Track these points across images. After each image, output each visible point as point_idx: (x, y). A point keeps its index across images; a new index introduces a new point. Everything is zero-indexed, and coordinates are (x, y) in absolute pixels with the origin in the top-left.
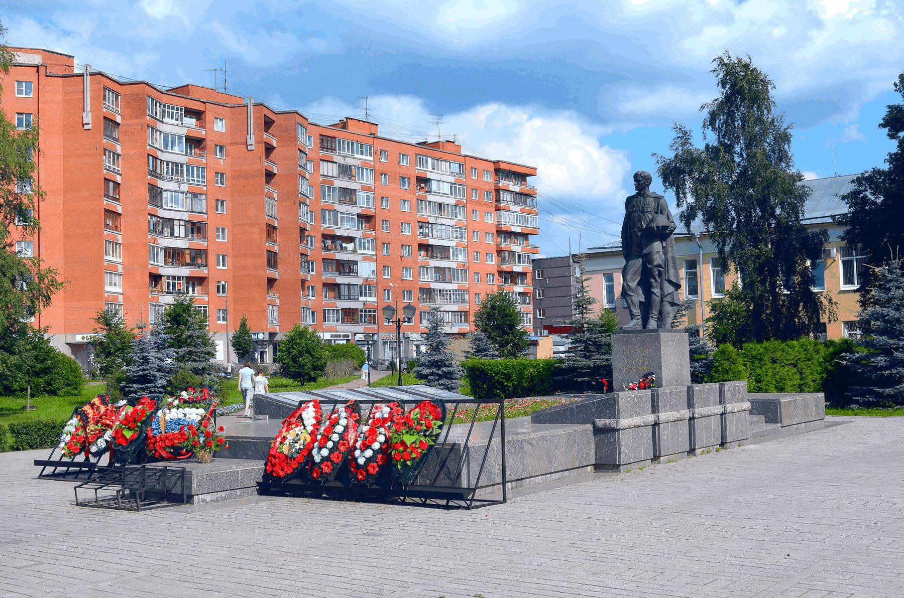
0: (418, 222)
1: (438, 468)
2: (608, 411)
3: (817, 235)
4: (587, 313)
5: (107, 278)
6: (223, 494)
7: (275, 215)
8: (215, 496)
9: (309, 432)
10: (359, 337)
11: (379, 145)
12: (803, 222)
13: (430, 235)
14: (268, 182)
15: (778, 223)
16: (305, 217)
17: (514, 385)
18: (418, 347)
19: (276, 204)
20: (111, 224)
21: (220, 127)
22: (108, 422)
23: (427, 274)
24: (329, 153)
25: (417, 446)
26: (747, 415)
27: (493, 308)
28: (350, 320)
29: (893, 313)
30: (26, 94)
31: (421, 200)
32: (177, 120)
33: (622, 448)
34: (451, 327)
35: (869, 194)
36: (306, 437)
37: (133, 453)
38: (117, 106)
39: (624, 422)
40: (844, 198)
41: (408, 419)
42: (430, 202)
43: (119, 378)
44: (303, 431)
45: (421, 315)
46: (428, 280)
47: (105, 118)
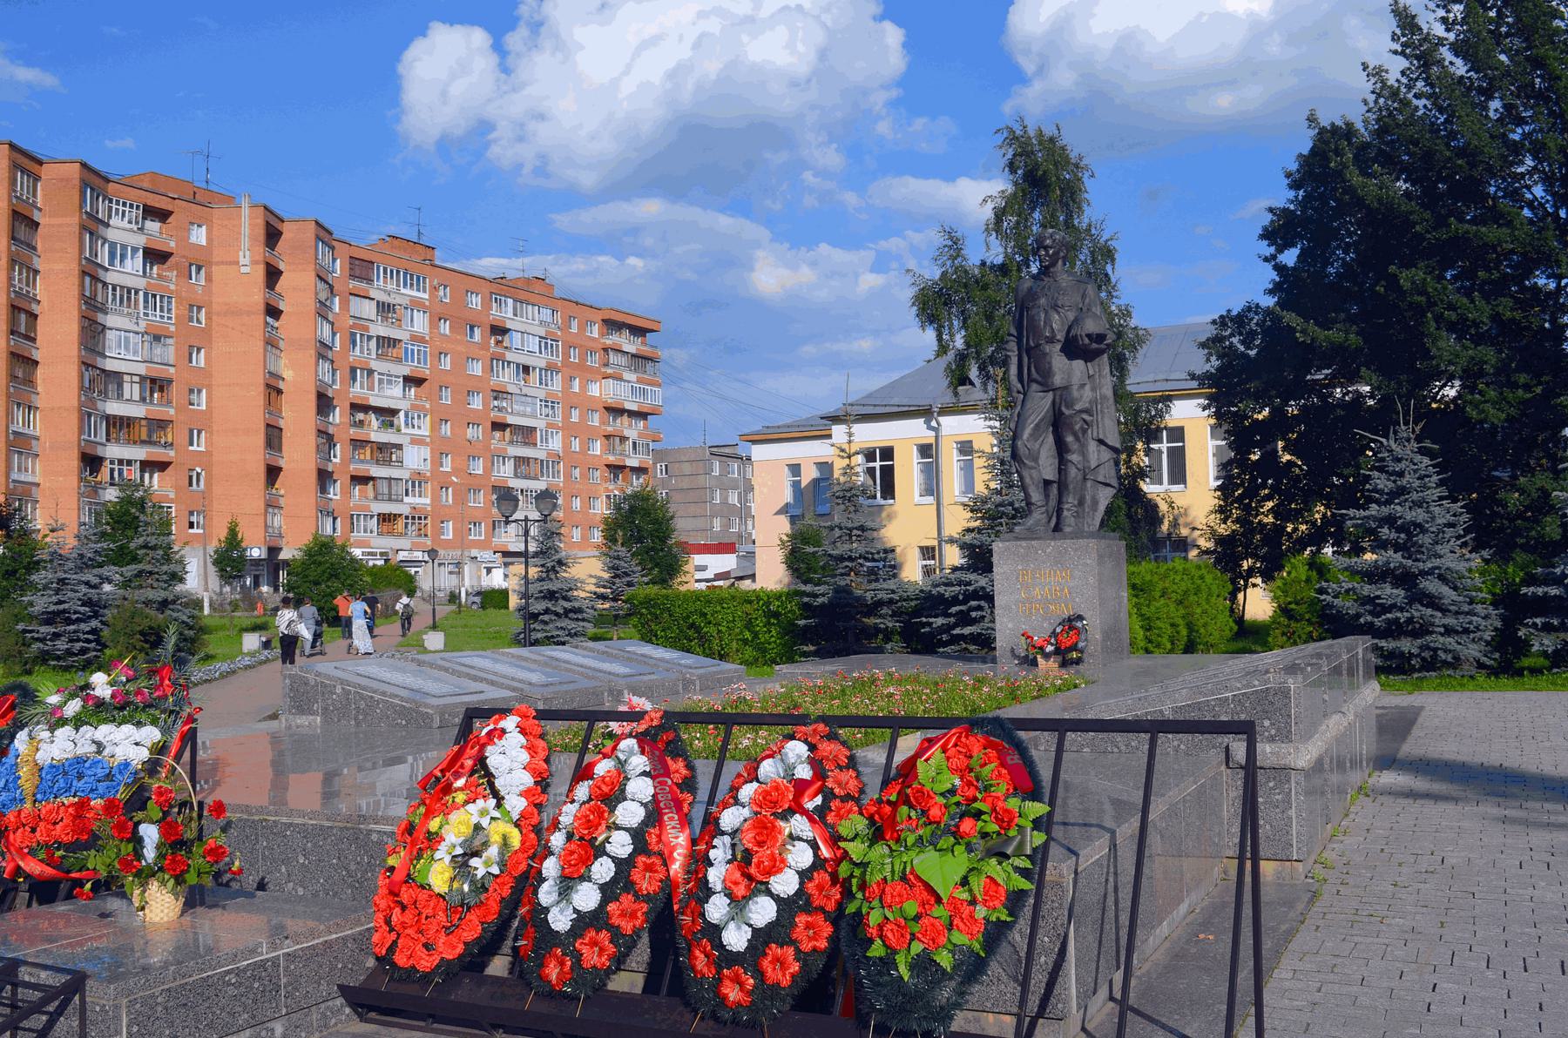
9: (515, 816)
24: (364, 285)
32: (130, 222)
36: (504, 833)
42: (509, 363)
46: (505, 472)
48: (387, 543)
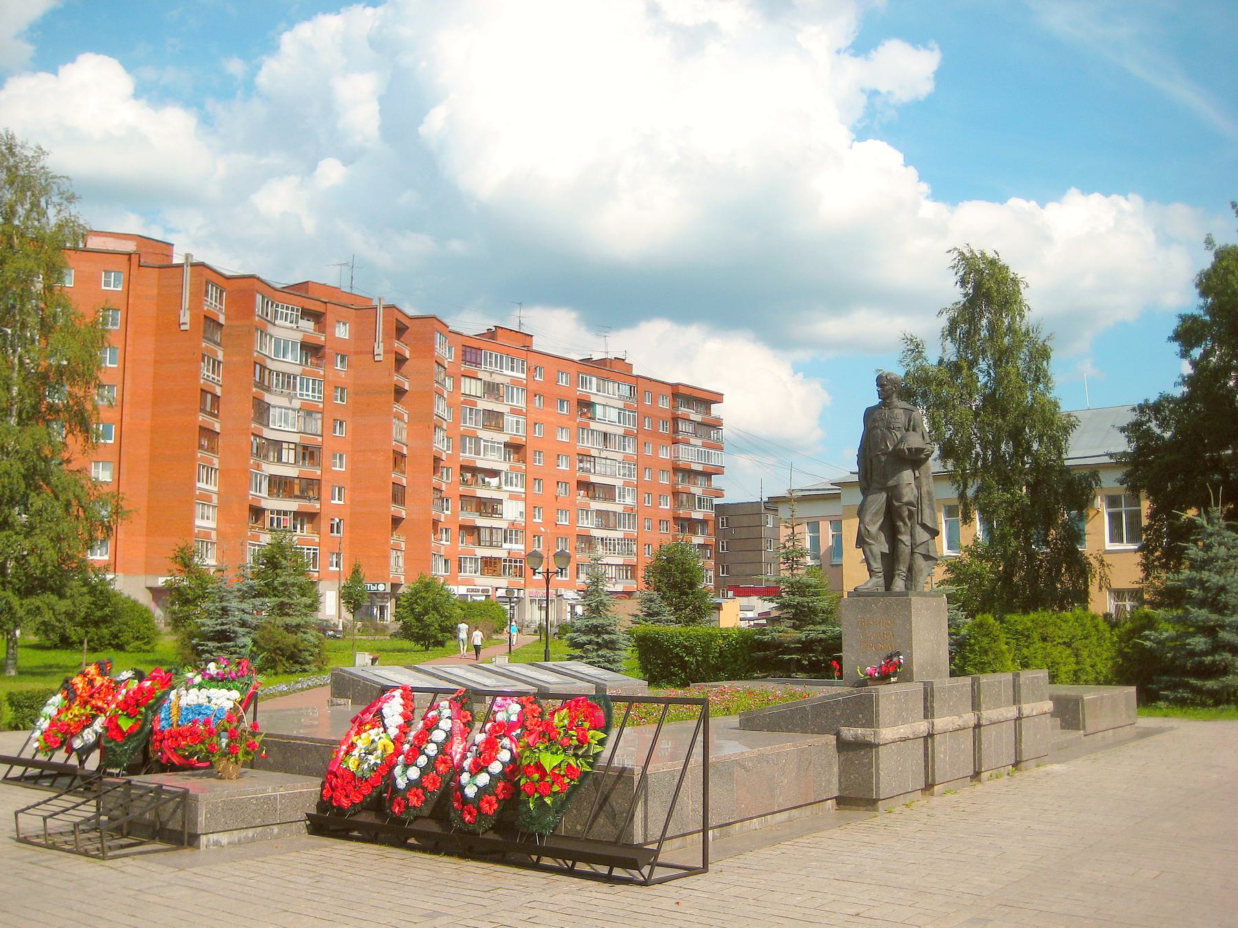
0: (578, 454)
1: (596, 807)
2: (861, 716)
3: (1085, 478)
4: (798, 569)
5: (199, 509)
6: (250, 833)
7: (404, 440)
8: (236, 836)
10: (501, 592)
11: (533, 360)
12: (1067, 463)
13: (593, 471)
14: (397, 400)
15: (1036, 460)
16: (440, 444)
17: (697, 661)
18: (573, 607)
19: (406, 426)
20: (206, 444)
21: (342, 332)
22: (100, 704)
23: (587, 519)
25: (562, 773)
26: (1048, 721)
27: (669, 561)
28: (490, 571)
29: (1216, 579)
30: (114, 287)
31: (584, 427)
32: (291, 322)
33: (882, 773)
34: (614, 584)
35: (1153, 425)
37: (132, 753)
38: (221, 304)
39: (887, 733)
40: (1123, 430)
41: (549, 727)
42: (593, 431)
43: (192, 632)
44: (383, 735)
45: (578, 569)
46: (587, 524)
47: (205, 316)
48: (489, 582)
